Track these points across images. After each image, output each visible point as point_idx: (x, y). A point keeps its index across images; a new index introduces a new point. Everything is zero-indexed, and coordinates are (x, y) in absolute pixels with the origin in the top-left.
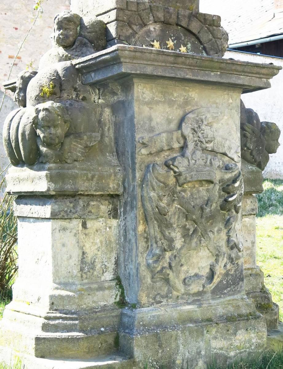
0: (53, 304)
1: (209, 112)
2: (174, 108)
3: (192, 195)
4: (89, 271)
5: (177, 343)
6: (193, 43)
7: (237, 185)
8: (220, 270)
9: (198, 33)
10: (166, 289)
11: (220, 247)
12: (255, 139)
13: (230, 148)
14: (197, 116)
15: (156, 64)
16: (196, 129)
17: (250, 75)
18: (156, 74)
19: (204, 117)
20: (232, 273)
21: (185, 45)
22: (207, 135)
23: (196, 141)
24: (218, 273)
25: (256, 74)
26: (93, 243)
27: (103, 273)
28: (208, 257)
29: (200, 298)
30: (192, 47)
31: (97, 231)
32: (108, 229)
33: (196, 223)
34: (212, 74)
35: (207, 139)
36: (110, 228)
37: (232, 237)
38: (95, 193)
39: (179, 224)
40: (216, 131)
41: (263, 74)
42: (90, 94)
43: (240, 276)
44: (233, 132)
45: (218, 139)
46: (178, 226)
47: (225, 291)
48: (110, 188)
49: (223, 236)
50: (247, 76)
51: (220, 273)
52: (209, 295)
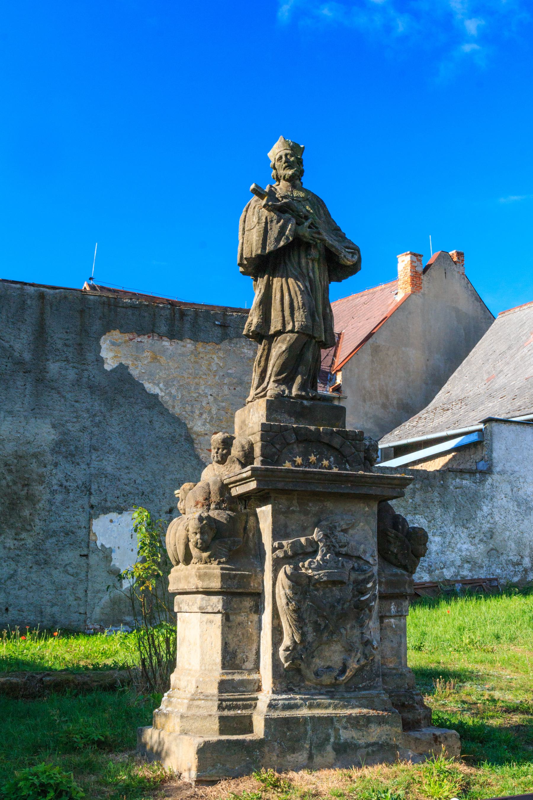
0: (198, 687)
1: (343, 519)
2: (309, 516)
3: (324, 594)
4: (231, 660)
5: (306, 728)
6: (336, 458)
7: (370, 585)
8: (353, 665)
9: (341, 447)
10: (298, 678)
11: (353, 643)
12: (400, 544)
13: (365, 552)
14: (331, 523)
15: (287, 480)
16: (329, 535)
17: (382, 486)
18: (287, 488)
19: (337, 524)
20: (367, 669)
21: (328, 459)
22: (341, 540)
23: (329, 546)
24: (351, 667)
25: (388, 484)
26: (235, 635)
27: (244, 662)
28: (341, 652)
29: (333, 690)
30: (335, 460)
31: (239, 624)
32: (250, 623)
33: (327, 620)
34: (343, 486)
35: (340, 544)
36: (251, 622)
37: (365, 634)
38: (236, 591)
39: (311, 619)
40: (351, 536)
41: (396, 485)
42: (237, 504)
43: (377, 672)
44: (369, 537)
45: (353, 543)
46: (309, 621)
47: (360, 686)
48: (251, 586)
49: (357, 632)
50: (379, 487)
51: (353, 668)
52: (342, 688)
